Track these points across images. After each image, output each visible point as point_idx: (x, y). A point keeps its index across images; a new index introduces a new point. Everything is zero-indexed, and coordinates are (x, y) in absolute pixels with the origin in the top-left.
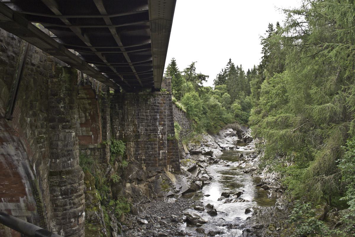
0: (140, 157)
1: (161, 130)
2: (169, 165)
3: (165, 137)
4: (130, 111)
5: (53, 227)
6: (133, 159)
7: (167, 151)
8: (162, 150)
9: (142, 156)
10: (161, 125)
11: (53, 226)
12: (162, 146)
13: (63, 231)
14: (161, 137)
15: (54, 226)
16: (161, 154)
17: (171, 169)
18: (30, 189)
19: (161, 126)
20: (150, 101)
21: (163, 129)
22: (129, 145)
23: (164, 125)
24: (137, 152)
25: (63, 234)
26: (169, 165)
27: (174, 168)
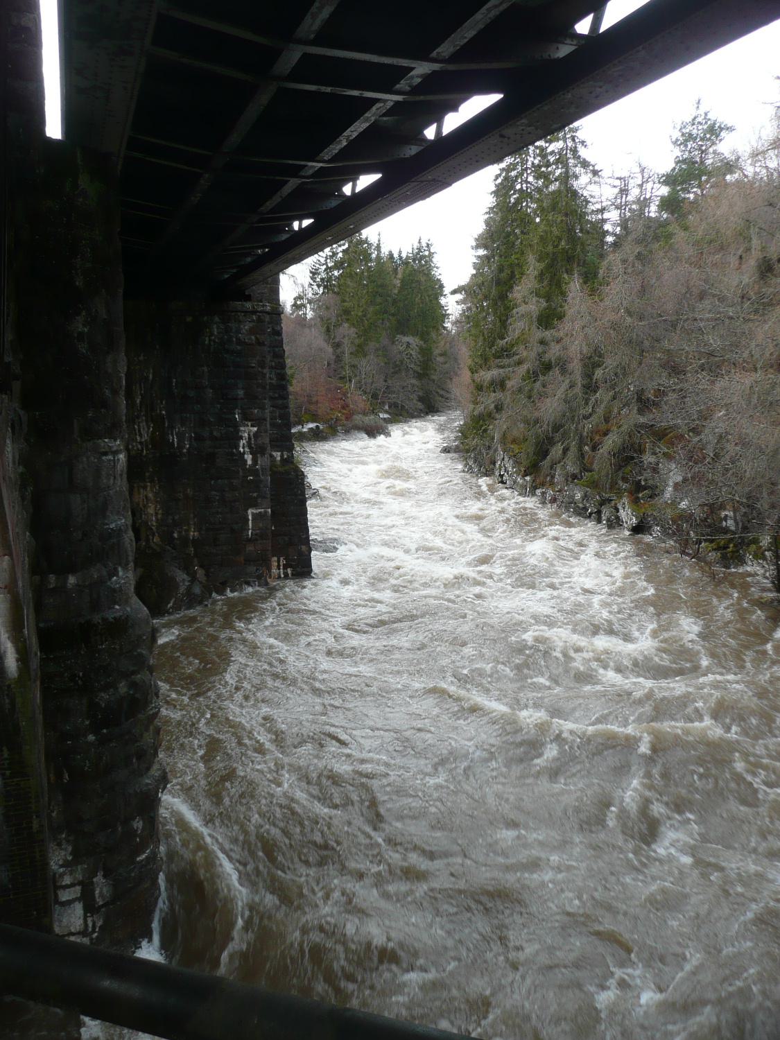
0: (180, 532)
1: (250, 438)
2: (276, 559)
3: (263, 462)
4: (137, 367)
5: (61, 870)
6: (156, 539)
7: (269, 510)
8: (255, 506)
9: (187, 531)
10: (250, 421)
11: (61, 866)
12: (255, 495)
13: (105, 876)
14: (249, 462)
15: (66, 864)
16: (250, 522)
17: (284, 569)
18: (220, 869)
19: (249, 424)
20: (212, 334)
21: (256, 435)
22: (142, 490)
23: (258, 422)
24: (170, 517)
25: (105, 890)
26: (276, 559)
27: (291, 566)
